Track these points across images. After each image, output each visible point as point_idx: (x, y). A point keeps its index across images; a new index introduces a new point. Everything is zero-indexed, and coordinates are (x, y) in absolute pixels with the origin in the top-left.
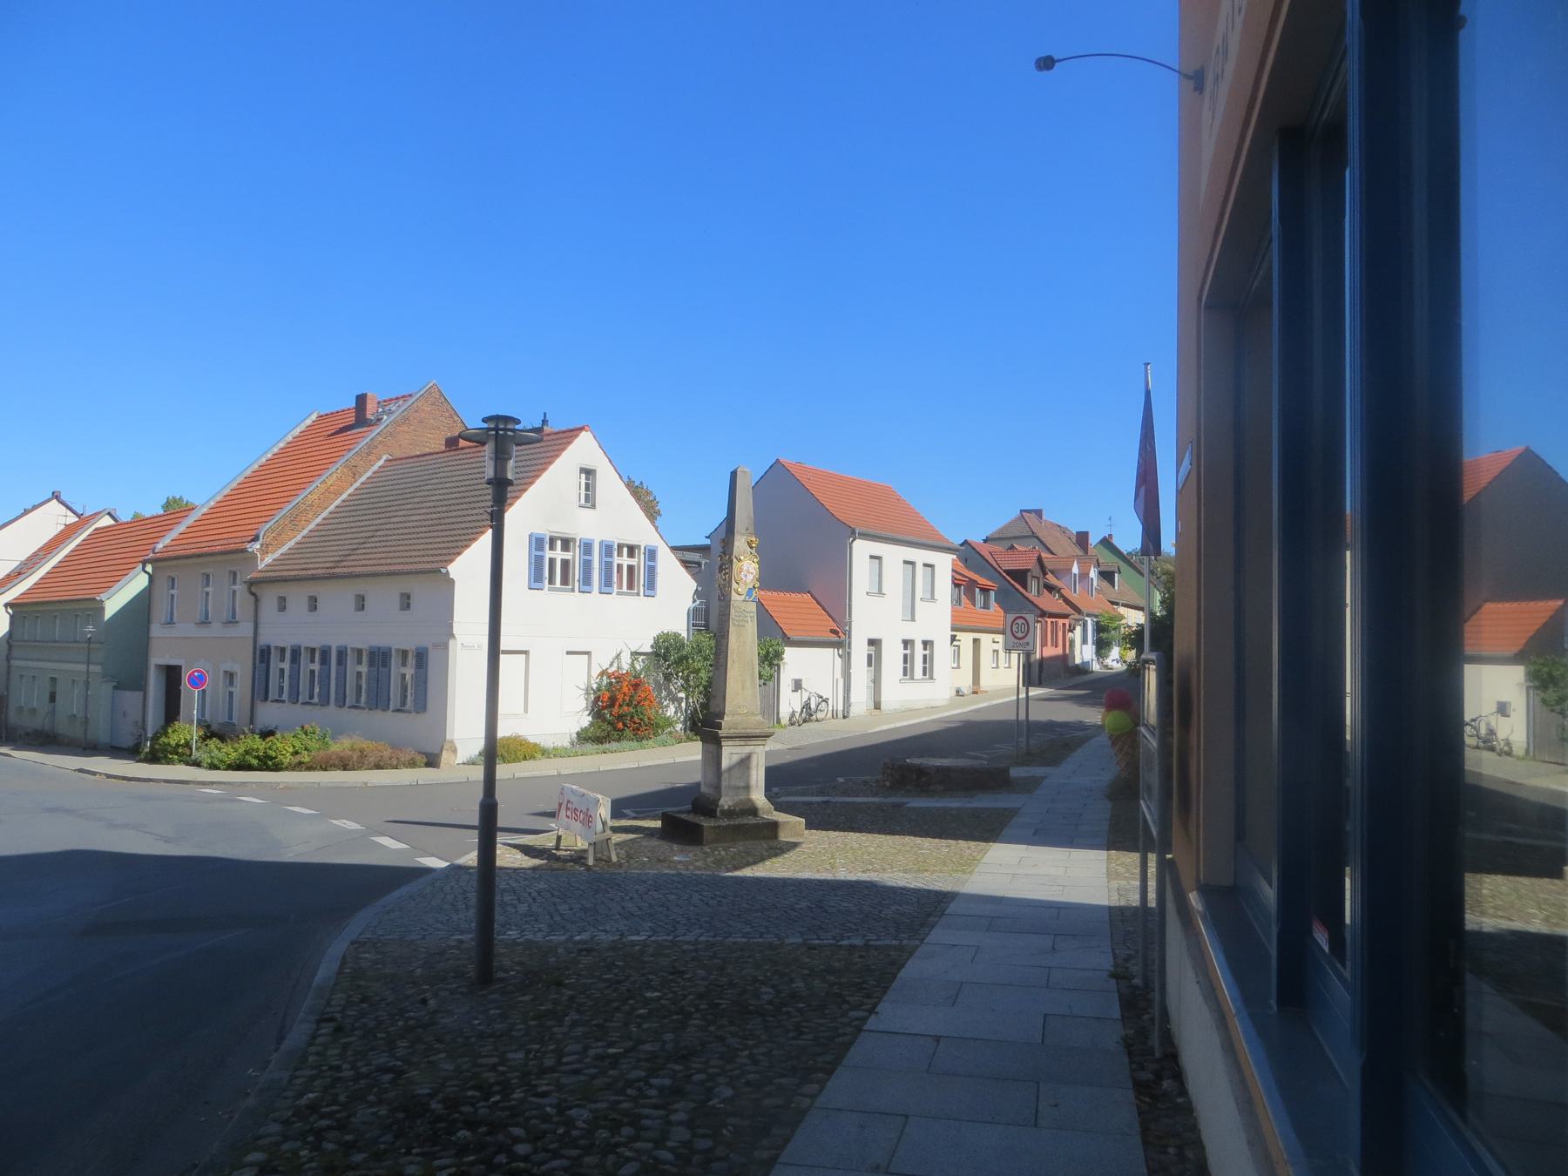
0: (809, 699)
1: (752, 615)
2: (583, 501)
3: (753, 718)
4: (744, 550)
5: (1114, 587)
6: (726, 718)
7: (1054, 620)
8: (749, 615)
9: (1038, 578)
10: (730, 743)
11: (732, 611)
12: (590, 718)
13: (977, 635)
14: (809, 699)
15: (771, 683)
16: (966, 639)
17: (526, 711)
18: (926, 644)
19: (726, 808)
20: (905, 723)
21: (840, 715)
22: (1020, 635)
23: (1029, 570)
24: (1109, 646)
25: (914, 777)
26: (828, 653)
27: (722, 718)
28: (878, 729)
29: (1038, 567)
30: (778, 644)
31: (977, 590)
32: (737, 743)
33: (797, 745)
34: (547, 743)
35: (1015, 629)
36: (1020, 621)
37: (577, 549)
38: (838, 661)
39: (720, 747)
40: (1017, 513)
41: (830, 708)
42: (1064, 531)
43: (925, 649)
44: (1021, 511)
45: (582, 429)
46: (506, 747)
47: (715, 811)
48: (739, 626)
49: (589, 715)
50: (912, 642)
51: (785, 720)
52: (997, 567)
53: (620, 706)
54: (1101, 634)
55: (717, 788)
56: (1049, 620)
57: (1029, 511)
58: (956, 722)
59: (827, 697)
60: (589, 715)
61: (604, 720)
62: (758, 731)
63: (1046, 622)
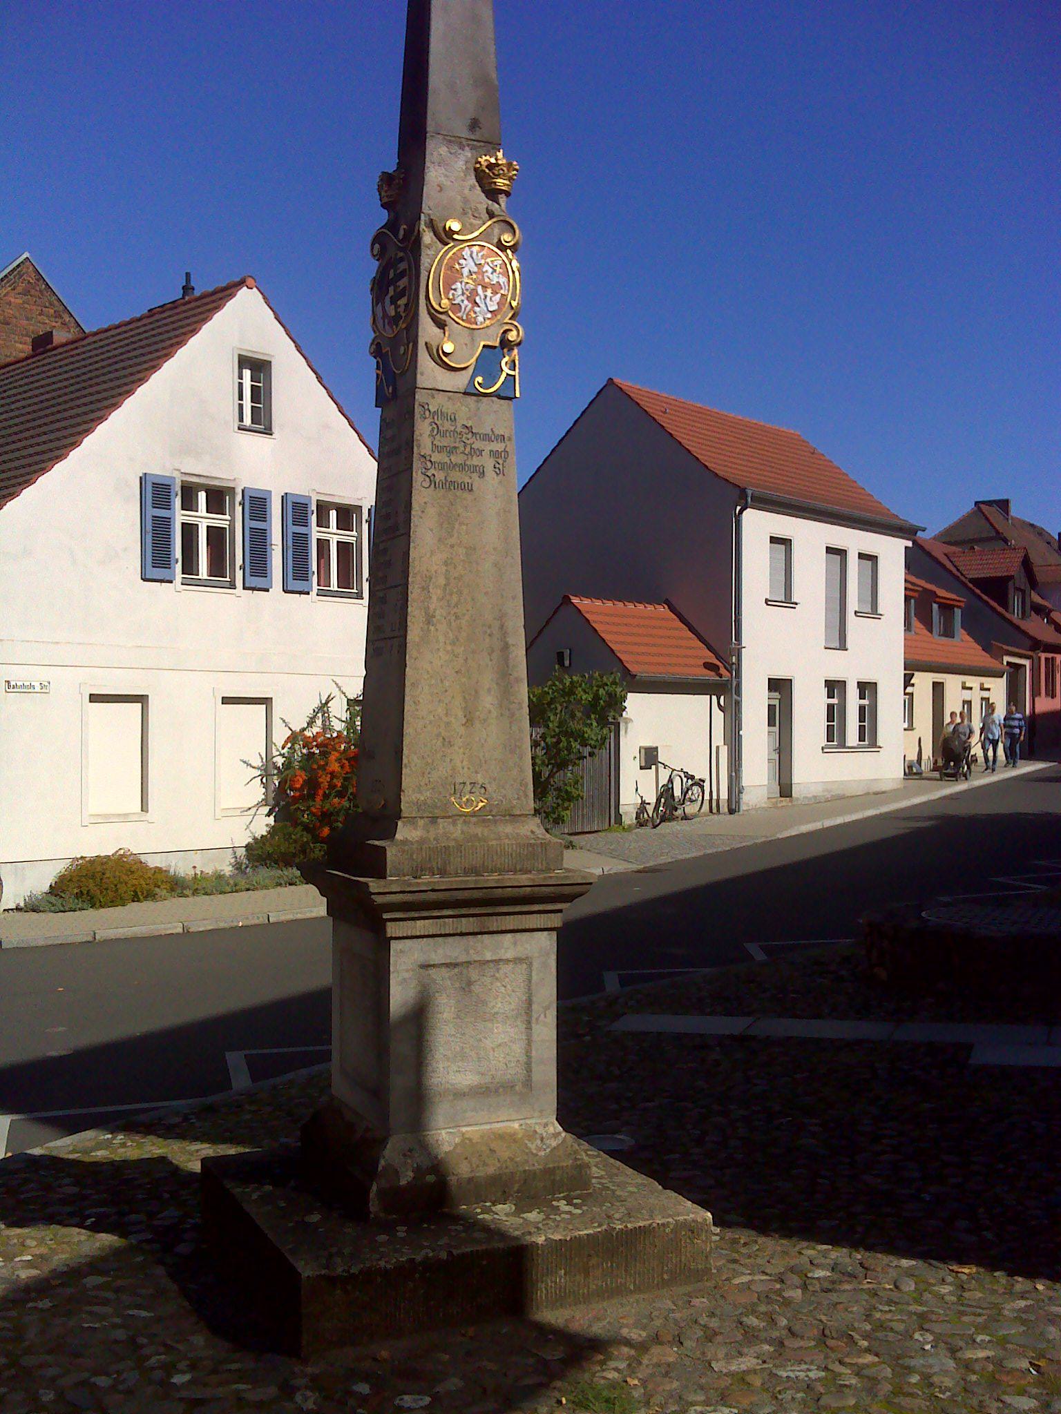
0: (671, 780)
1: (499, 446)
2: (247, 421)
3: (508, 829)
4: (466, 200)
6: (404, 832)
7: (1050, 655)
9: (1023, 592)
10: (421, 926)
12: (271, 820)
13: (939, 677)
14: (671, 780)
15: (604, 752)
16: (924, 681)
17: (144, 807)
19: (406, 1178)
20: (839, 820)
21: (724, 808)
23: (1011, 577)
26: (701, 702)
27: (390, 834)
28: (793, 832)
29: (1023, 574)
30: (614, 683)
31: (935, 606)
32: (449, 925)
33: (651, 864)
34: (182, 868)
37: (239, 509)
38: (718, 716)
39: (384, 943)
40: (969, 507)
41: (707, 797)
42: (1041, 533)
43: (862, 697)
44: (976, 503)
45: (241, 283)
46: (98, 876)
48: (449, 485)
49: (268, 815)
50: (842, 684)
51: (629, 817)
52: (959, 574)
53: (326, 796)
56: (1043, 656)
57: (989, 503)
58: (930, 818)
59: (702, 777)
60: (268, 815)
61: (295, 823)
62: (524, 879)
63: (1040, 658)
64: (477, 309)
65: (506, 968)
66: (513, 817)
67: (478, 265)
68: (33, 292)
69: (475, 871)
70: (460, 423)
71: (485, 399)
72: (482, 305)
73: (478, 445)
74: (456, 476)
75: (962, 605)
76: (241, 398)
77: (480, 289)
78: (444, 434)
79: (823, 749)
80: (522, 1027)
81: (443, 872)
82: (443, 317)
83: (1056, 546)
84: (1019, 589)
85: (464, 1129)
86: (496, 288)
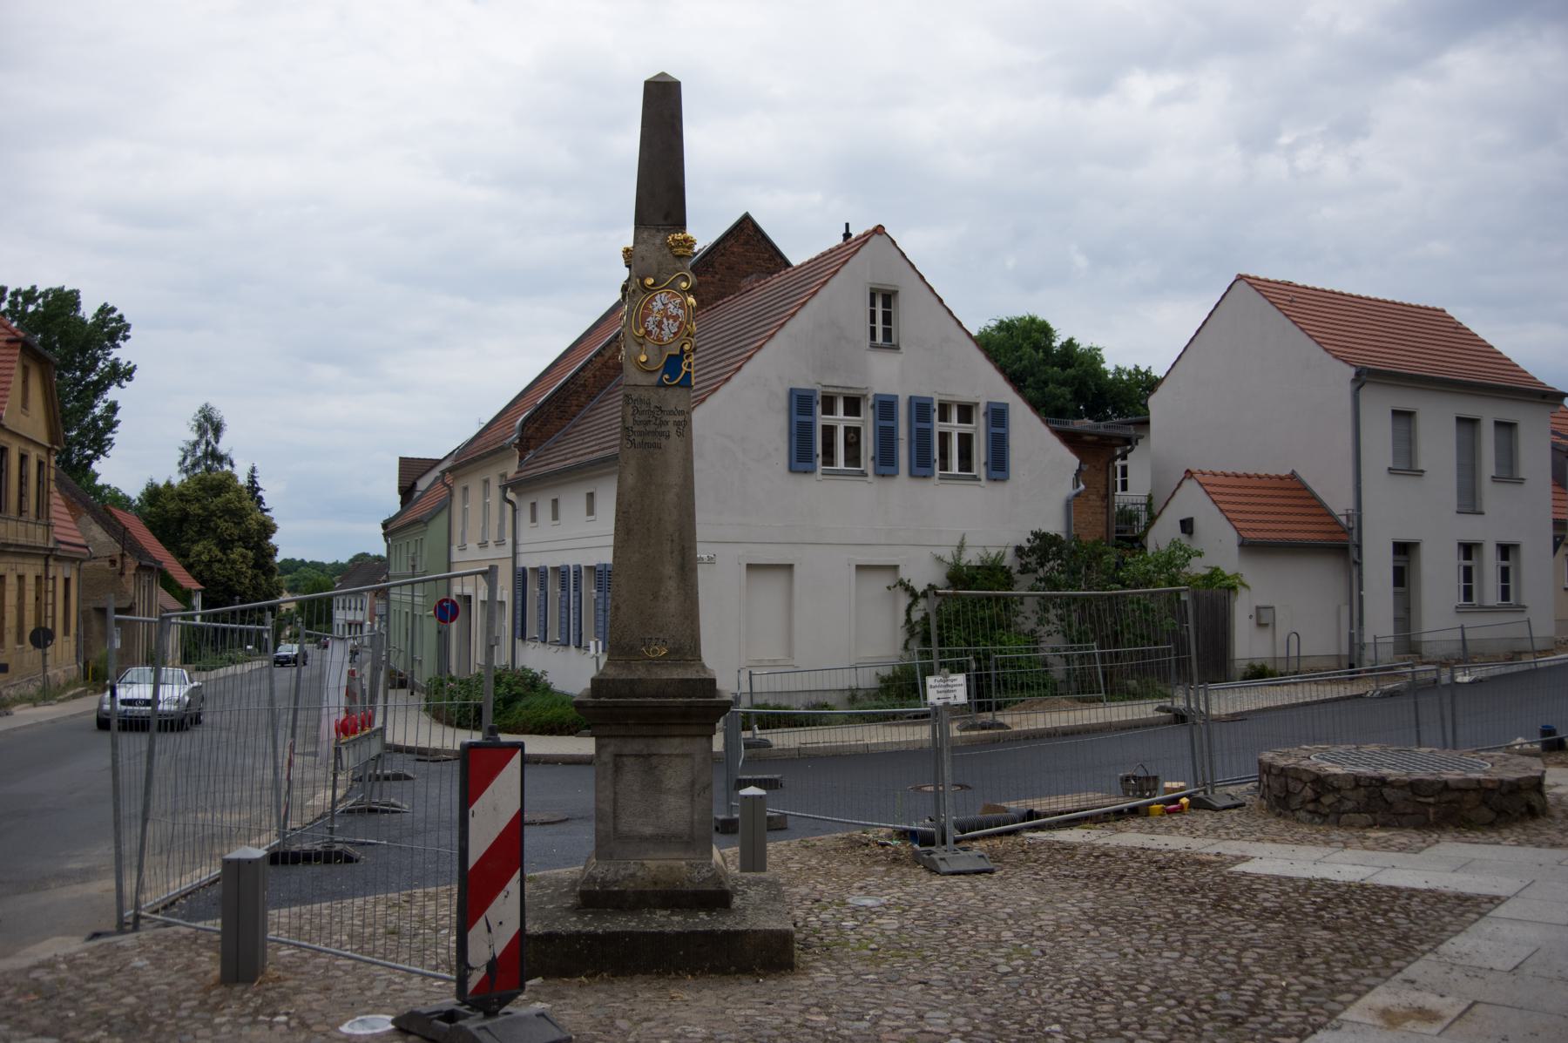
8: (671, 419)
18: (1506, 550)
25: (1308, 793)
48: (644, 445)
68: (752, 242)
71: (670, 389)
73: (666, 418)
74: (649, 439)
76: (873, 320)
77: (665, 320)
78: (642, 413)
86: (676, 318)
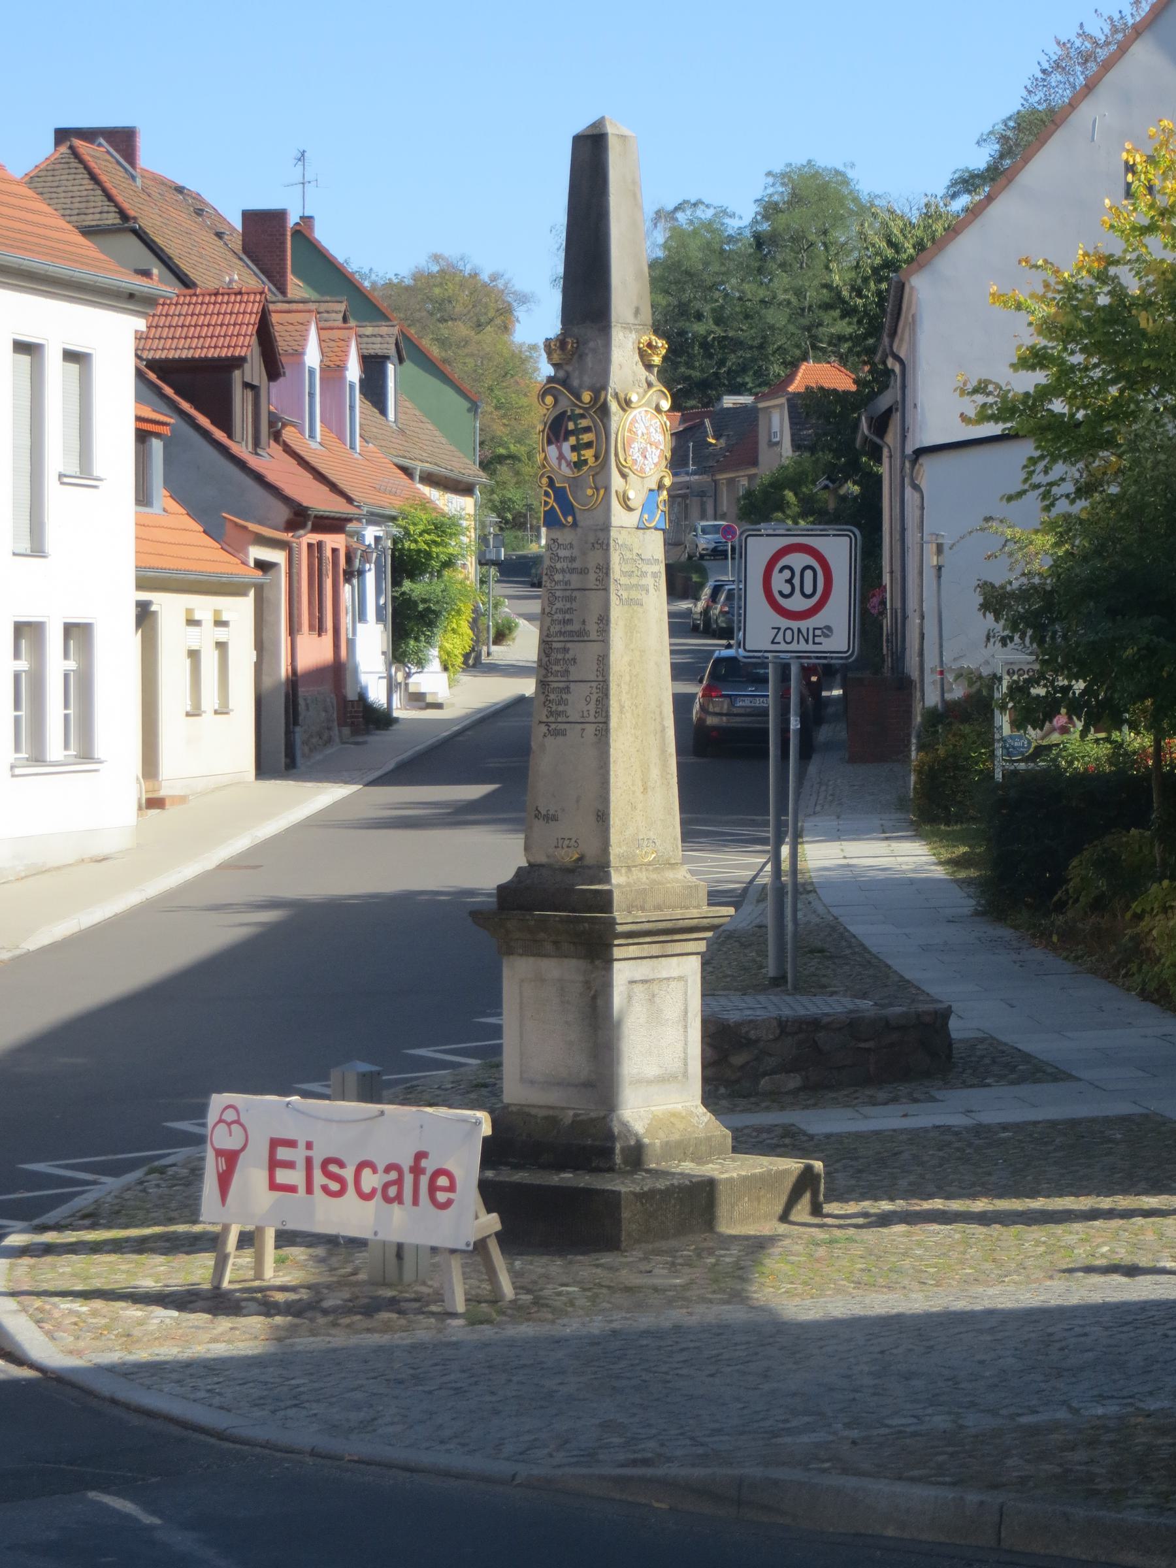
5: (383, 411)
7: (314, 538)
11: (615, 558)
22: (797, 603)
24: (431, 624)
27: (606, 879)
35: (779, 582)
36: (798, 560)
44: (62, 135)
47: (611, 1151)
54: (407, 585)
55: (588, 1085)
57: (88, 135)
64: (646, 462)
65: (673, 984)
66: (672, 866)
67: (647, 428)
69: (659, 908)
70: (635, 551)
72: (650, 459)
73: (645, 568)
75: (166, 431)
79: (12, 767)
80: (682, 1030)
81: (643, 909)
82: (626, 470)
83: (237, 243)
84: (247, 385)
85: (653, 1108)
